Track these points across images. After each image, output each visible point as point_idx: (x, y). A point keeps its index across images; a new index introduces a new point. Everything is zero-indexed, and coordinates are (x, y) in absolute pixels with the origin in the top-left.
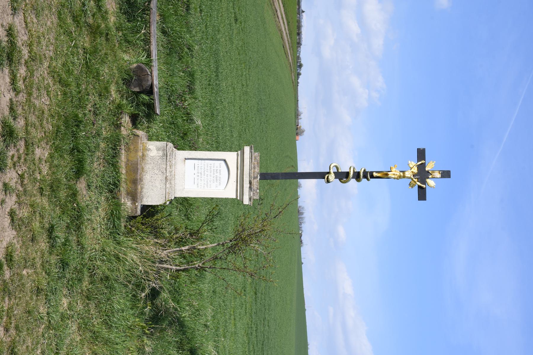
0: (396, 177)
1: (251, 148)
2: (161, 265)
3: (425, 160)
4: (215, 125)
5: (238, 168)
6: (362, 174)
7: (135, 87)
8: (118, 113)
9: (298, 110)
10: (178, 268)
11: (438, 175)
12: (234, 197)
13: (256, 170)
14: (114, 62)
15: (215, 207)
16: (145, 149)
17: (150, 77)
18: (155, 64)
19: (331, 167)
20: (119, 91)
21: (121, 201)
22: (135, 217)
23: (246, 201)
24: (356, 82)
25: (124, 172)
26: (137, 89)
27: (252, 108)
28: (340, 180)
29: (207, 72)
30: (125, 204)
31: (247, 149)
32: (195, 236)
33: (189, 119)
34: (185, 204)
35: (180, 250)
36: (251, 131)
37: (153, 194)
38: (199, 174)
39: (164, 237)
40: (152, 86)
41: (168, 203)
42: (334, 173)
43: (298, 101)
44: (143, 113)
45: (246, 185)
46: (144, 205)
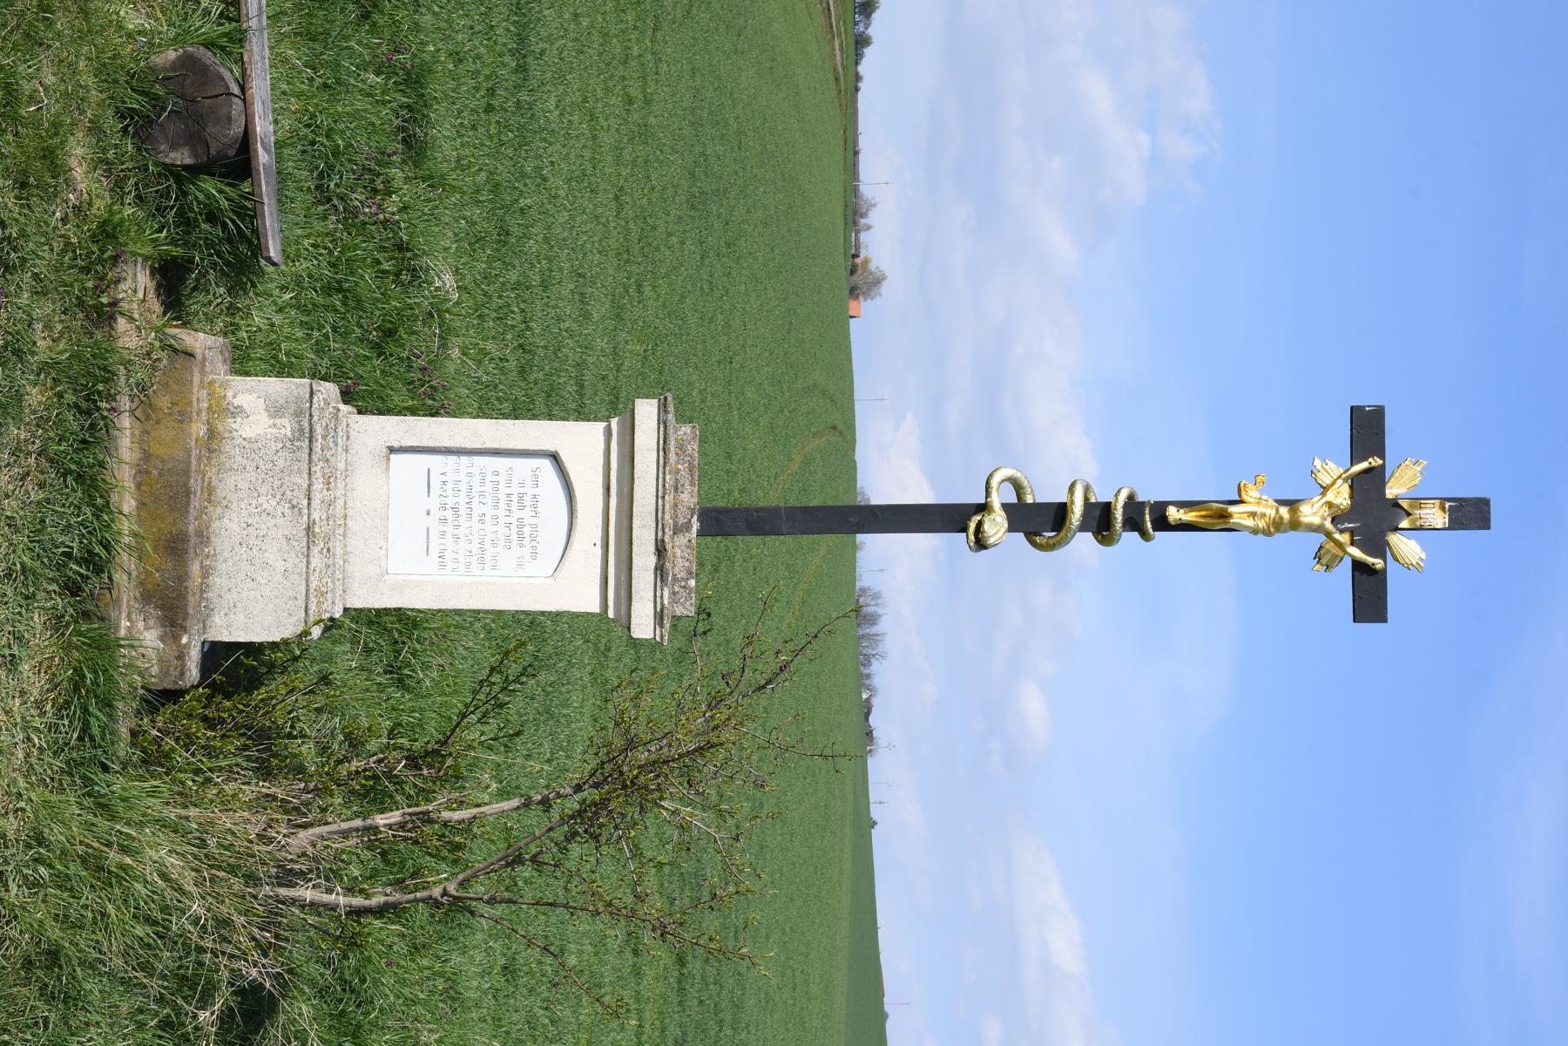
0: (1261, 524)
1: (663, 408)
2: (283, 891)
3: (1382, 456)
4: (513, 276)
5: (607, 489)
6: (1119, 514)
7: (173, 147)
8: (100, 261)
9: (856, 190)
10: (358, 901)
11: (1436, 517)
12: (594, 607)
13: (685, 497)
14: (82, 36)
15: (520, 645)
16: (221, 410)
17: (237, 104)
18: (259, 52)
19: (995, 483)
20: (103, 164)
21: (117, 629)
22: (172, 695)
23: (643, 626)
24: (1098, 94)
25: (128, 504)
26: (182, 157)
27: (670, 192)
28: (1030, 536)
29: (479, 57)
30: (133, 642)
31: (646, 411)
32: (430, 766)
33: (405, 263)
34: (392, 634)
35: (367, 829)
36: (663, 290)
37: (253, 598)
38: (449, 514)
39: (300, 770)
40: (245, 143)
41: (316, 632)
42: (1005, 507)
43: (856, 153)
44: (207, 259)
45: (644, 561)
46: (214, 644)
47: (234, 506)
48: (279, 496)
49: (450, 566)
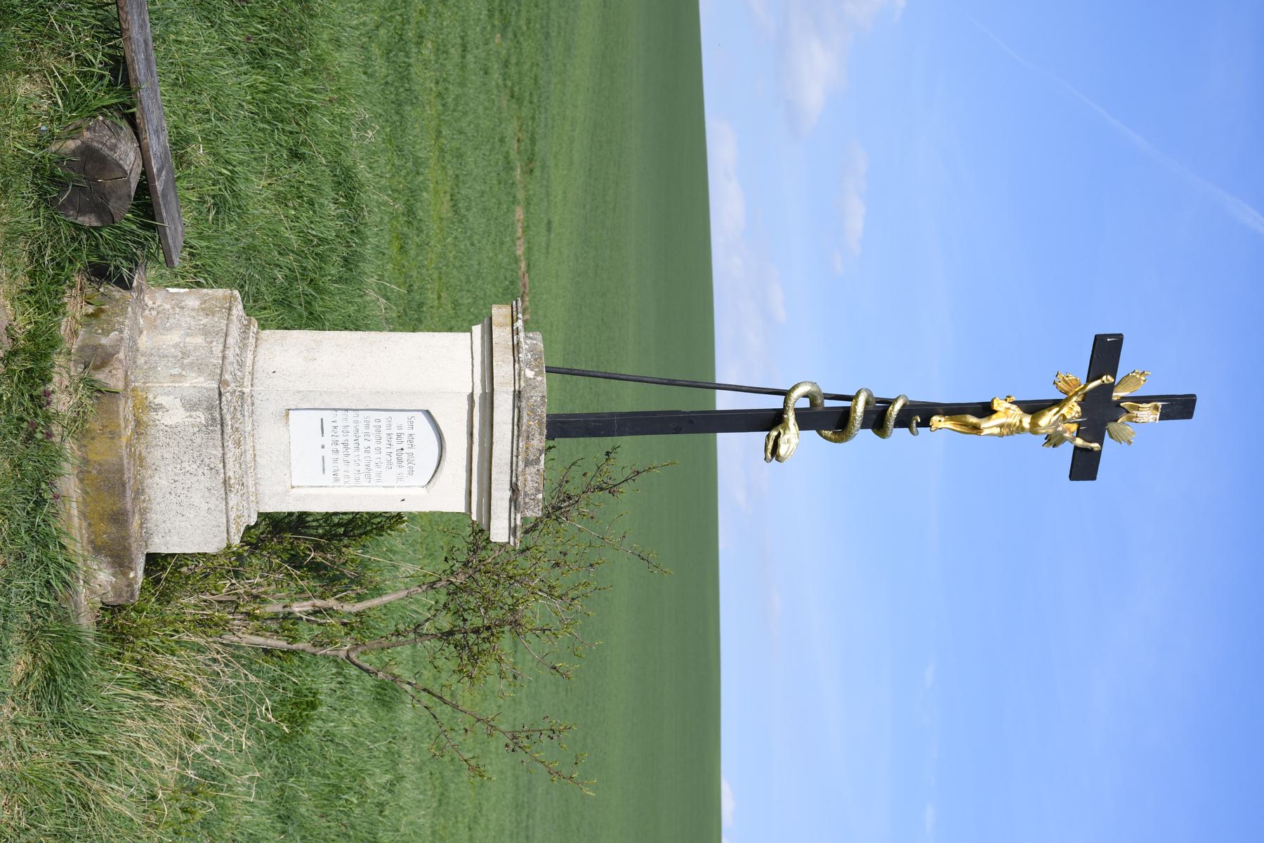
5: (471, 435)
23: (499, 532)
37: (188, 517)
38: (340, 447)
47: (162, 469)
48: (198, 462)
49: (342, 480)
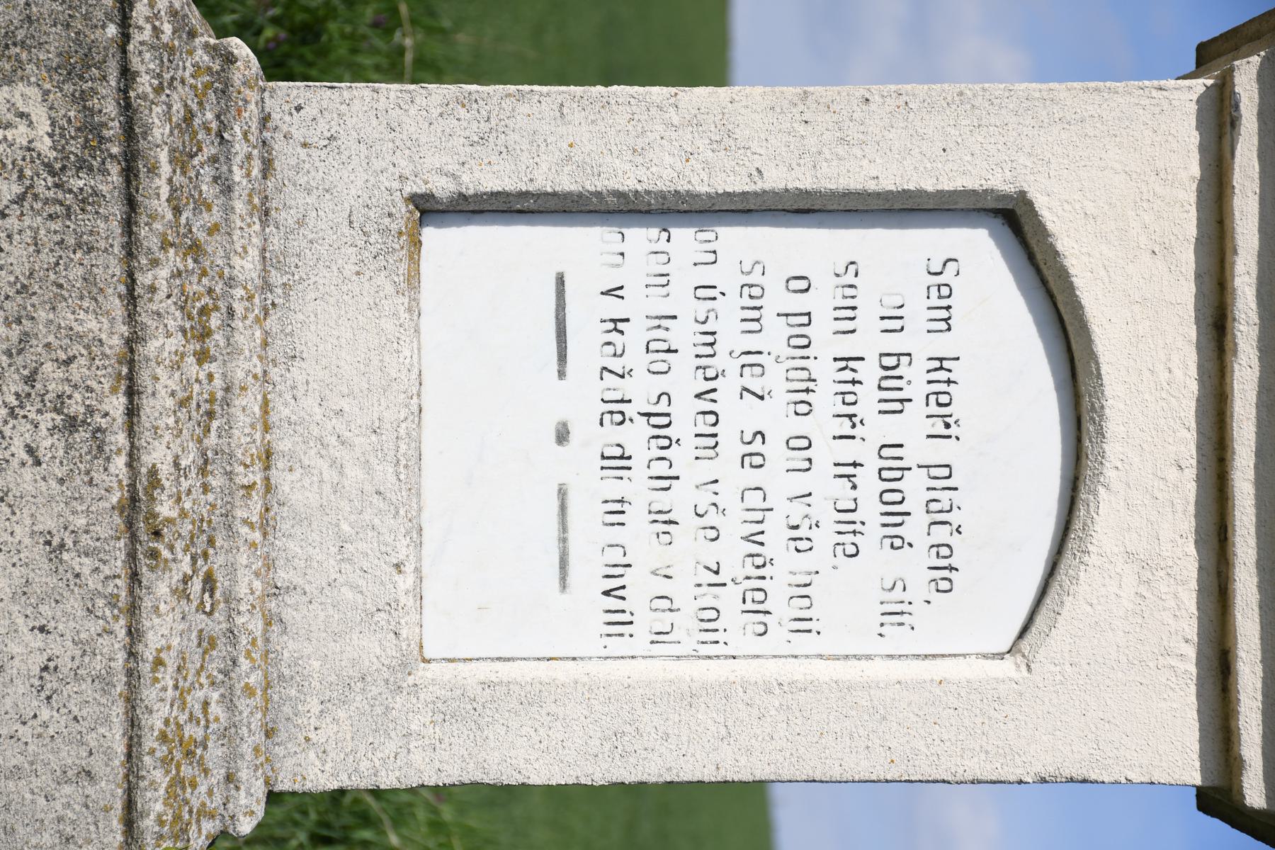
38: (636, 436)
